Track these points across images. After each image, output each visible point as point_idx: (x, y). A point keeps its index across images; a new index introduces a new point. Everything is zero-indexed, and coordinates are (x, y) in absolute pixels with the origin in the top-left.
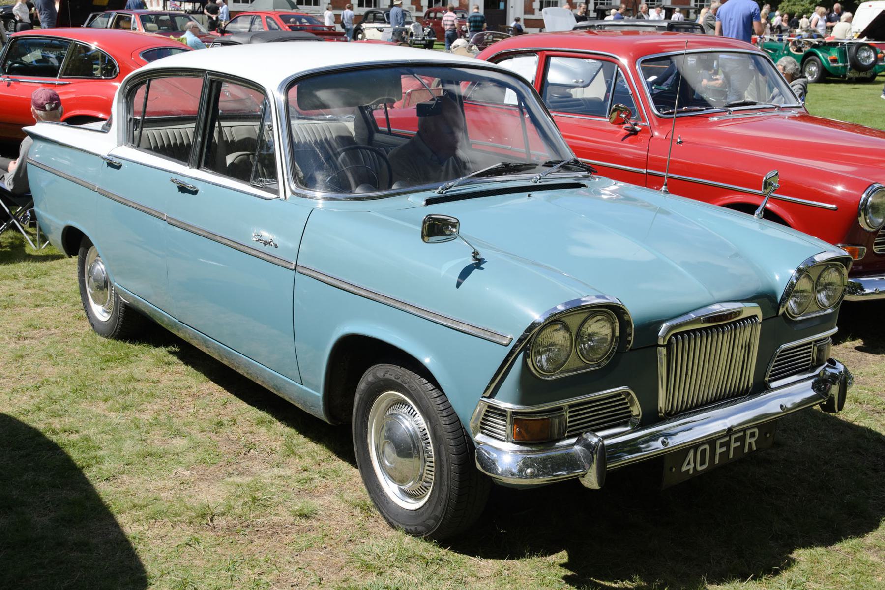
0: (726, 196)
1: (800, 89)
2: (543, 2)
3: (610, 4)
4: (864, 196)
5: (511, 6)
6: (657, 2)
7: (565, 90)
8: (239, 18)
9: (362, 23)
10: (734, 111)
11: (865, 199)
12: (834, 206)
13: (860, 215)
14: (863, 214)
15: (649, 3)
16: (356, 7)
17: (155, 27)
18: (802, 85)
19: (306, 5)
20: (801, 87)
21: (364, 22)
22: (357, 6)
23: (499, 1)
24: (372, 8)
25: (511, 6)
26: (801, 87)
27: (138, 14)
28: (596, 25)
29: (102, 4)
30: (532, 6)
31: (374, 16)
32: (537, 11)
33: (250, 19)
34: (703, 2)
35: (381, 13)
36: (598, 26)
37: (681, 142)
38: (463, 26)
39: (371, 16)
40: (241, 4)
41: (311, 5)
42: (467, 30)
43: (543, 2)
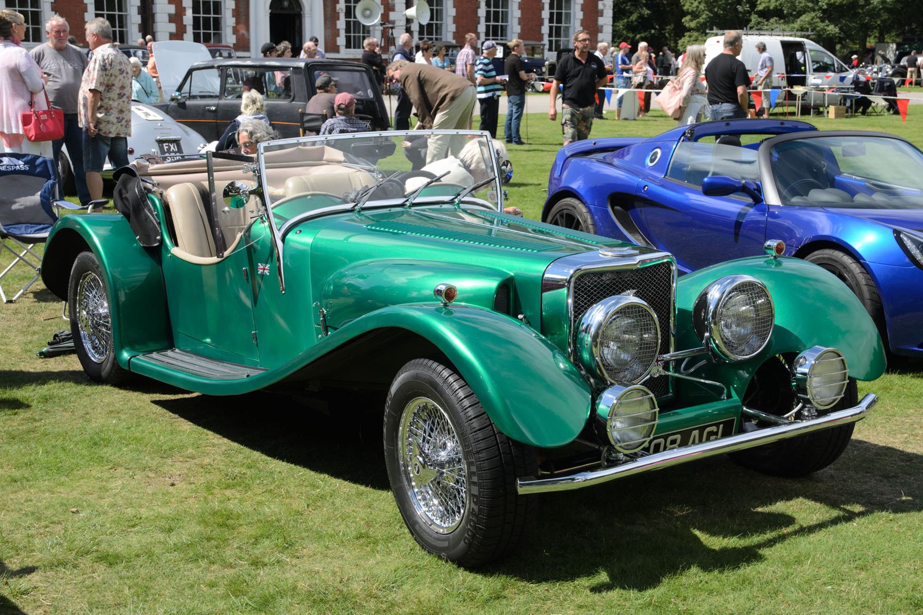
15: (491, 38)
30: (336, 42)
32: (343, 49)
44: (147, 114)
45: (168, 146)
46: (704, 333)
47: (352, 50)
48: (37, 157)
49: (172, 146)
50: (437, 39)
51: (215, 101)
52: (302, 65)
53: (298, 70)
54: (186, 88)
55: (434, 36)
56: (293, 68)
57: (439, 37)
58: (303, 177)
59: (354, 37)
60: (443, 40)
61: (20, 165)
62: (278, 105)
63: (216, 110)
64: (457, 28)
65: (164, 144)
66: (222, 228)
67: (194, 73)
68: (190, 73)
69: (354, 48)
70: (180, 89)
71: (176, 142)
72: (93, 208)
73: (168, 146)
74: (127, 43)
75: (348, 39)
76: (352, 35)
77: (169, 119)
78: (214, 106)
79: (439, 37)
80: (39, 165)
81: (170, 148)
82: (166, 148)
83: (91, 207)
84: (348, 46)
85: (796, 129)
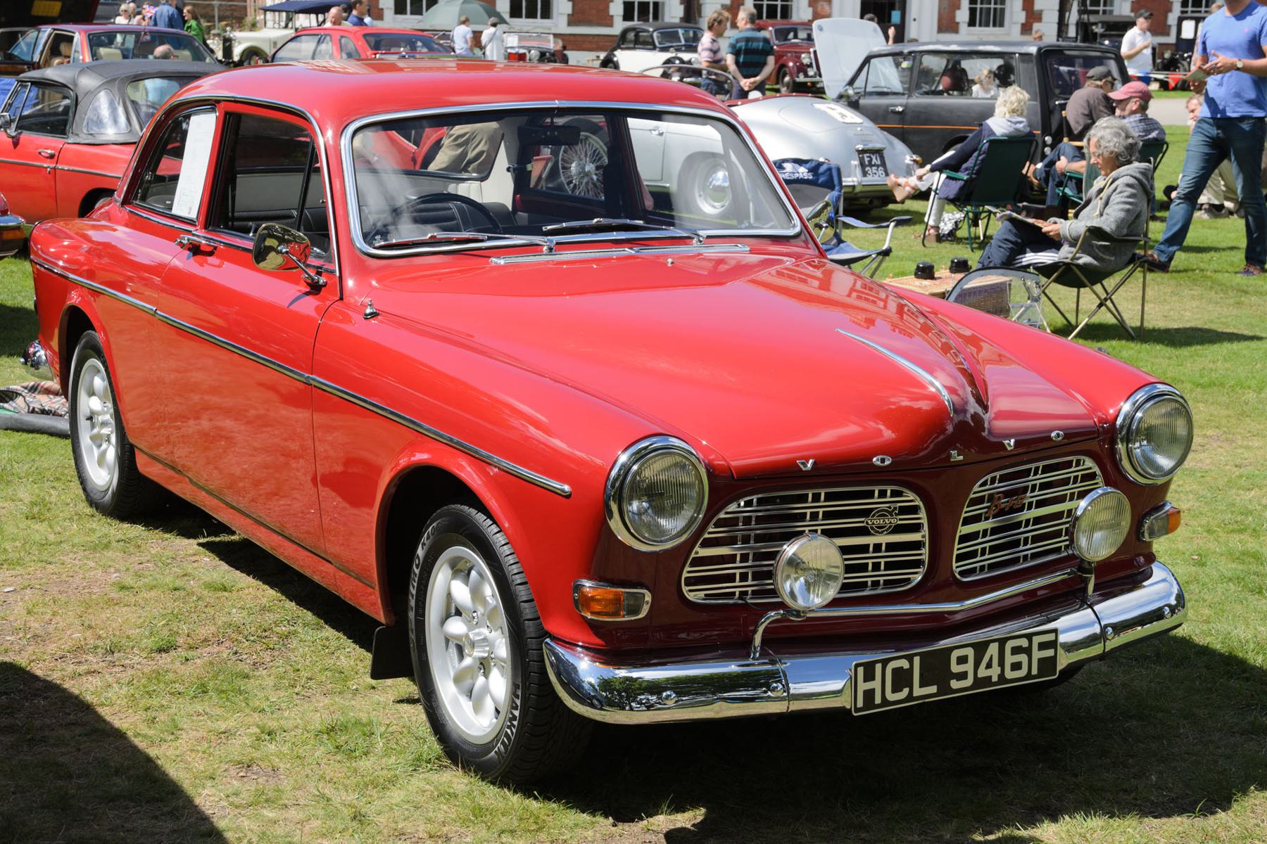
0: (556, 451)
1: (1129, 185)
2: (633, 3)
3: (1111, 12)
4: (623, 458)
5: (912, 18)
6: (982, 3)
7: (446, 188)
8: (303, 37)
9: (615, 49)
10: (709, 237)
11: (623, 465)
12: (567, 488)
13: (611, 516)
14: (614, 507)
15: (1190, 9)
16: (389, 13)
17: (114, 54)
18: (1135, 178)
19: (412, 13)
20: (1132, 181)
21: (618, 47)
22: (621, 18)
23: (892, 7)
24: (635, 23)
25: (912, 18)
26: (1132, 181)
27: (85, 31)
28: (906, 51)
29: (50, 14)
30: (954, 17)
31: (637, 36)
32: (964, 28)
33: (317, 38)
34: (976, 4)
35: (648, 31)
36: (910, 53)
37: (374, 315)
38: (803, 55)
39: (631, 36)
40: (408, 16)
41: (520, 16)
42: (811, 63)
43: (633, 3)
44: (843, 116)
45: (870, 157)
46: (873, 465)
47: (977, 29)
48: (820, 164)
49: (874, 158)
50: (1104, 12)
51: (903, 100)
52: (1033, 50)
53: (1026, 57)
54: (860, 83)
55: (1101, 8)
56: (1020, 54)
57: (1108, 8)
58: (383, 243)
59: (995, 9)
60: (1116, 13)
61: (803, 172)
62: (932, 106)
63: (903, 111)
64: (608, 7)
65: (865, 155)
66: (104, 323)
67: (873, 61)
68: (867, 60)
69: (994, 25)
70: (851, 82)
71: (879, 152)
72: (896, 226)
73: (870, 157)
74: (663, 20)
75: (972, 12)
76: (979, 6)
77: (869, 124)
78: (901, 105)
79: (1108, 8)
80: (823, 174)
81: (871, 159)
82: (867, 160)
83: (892, 224)
84: (972, 23)
85: (205, 237)
